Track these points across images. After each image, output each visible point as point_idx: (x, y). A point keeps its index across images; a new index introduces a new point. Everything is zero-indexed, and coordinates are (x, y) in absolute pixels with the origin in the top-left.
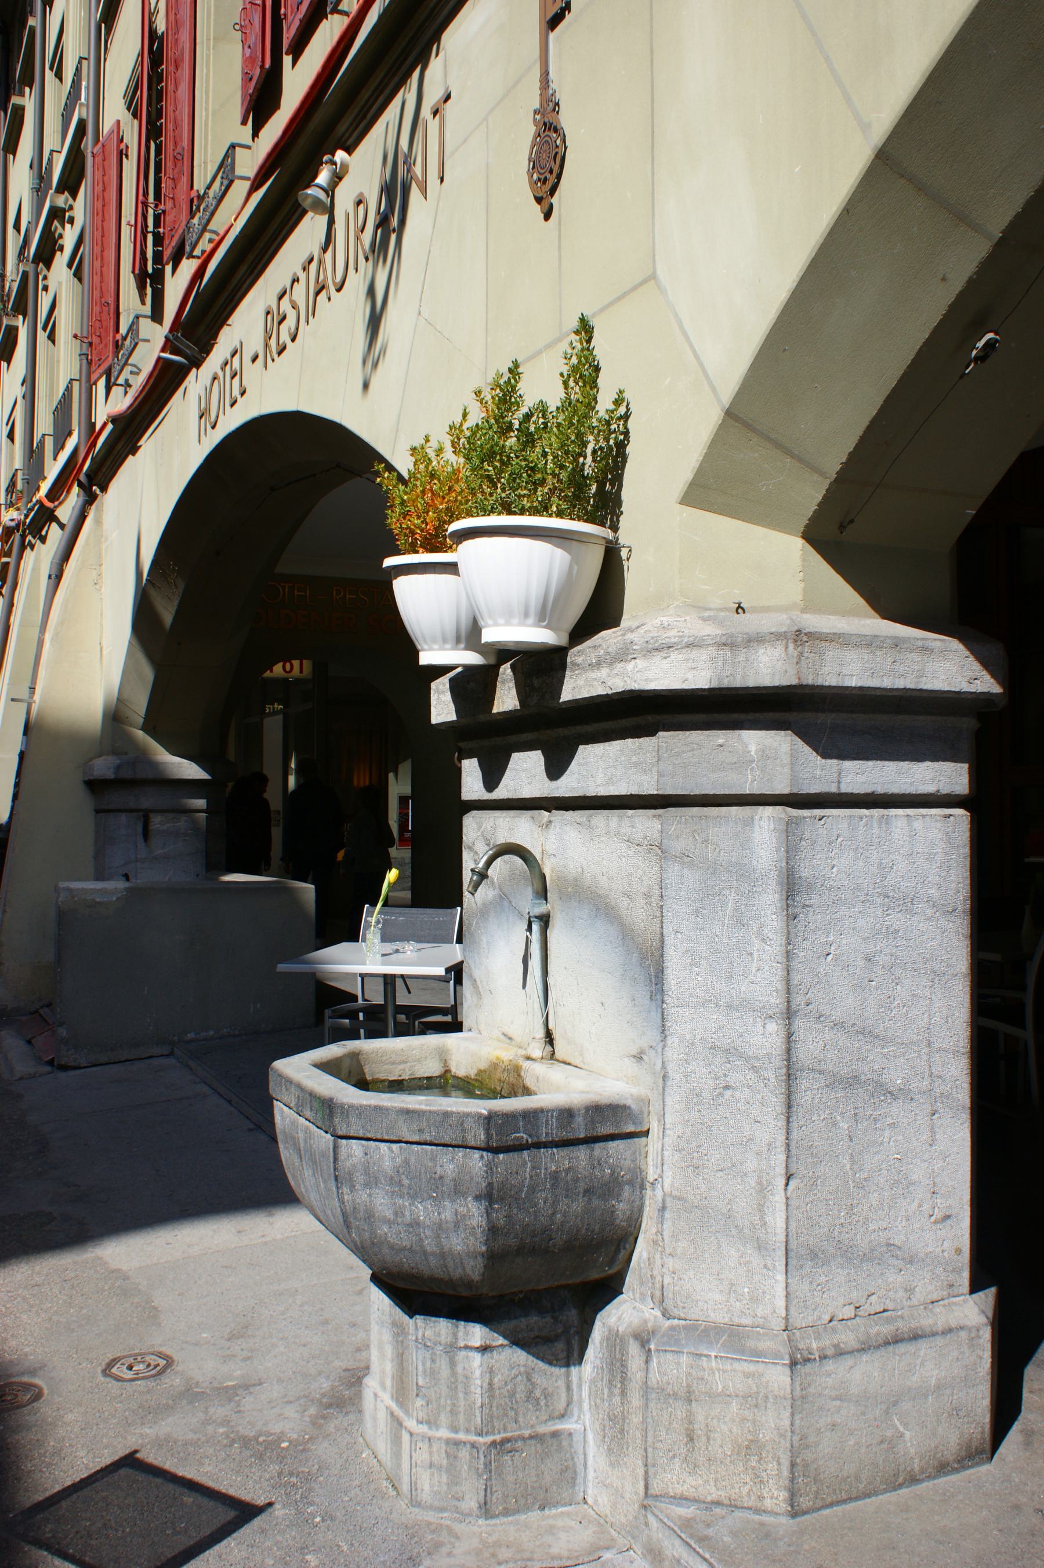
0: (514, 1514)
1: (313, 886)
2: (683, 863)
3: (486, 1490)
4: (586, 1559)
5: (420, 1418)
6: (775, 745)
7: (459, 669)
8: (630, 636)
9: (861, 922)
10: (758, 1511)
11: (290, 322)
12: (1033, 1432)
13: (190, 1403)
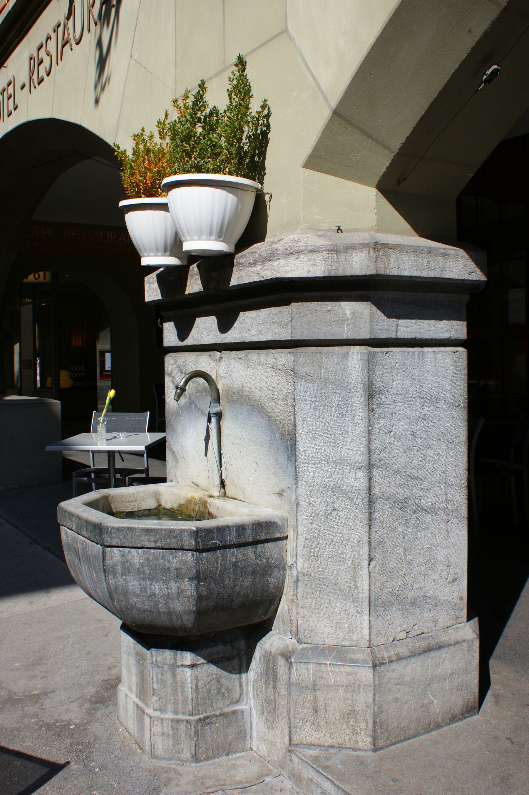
0: (212, 759)
1: (59, 402)
2: (307, 380)
3: (196, 746)
4: (256, 783)
5: (155, 708)
6: (361, 310)
7: (162, 269)
8: (274, 246)
9: (409, 413)
10: (355, 749)
11: (46, 63)
12: (498, 695)
13: (12, 705)
